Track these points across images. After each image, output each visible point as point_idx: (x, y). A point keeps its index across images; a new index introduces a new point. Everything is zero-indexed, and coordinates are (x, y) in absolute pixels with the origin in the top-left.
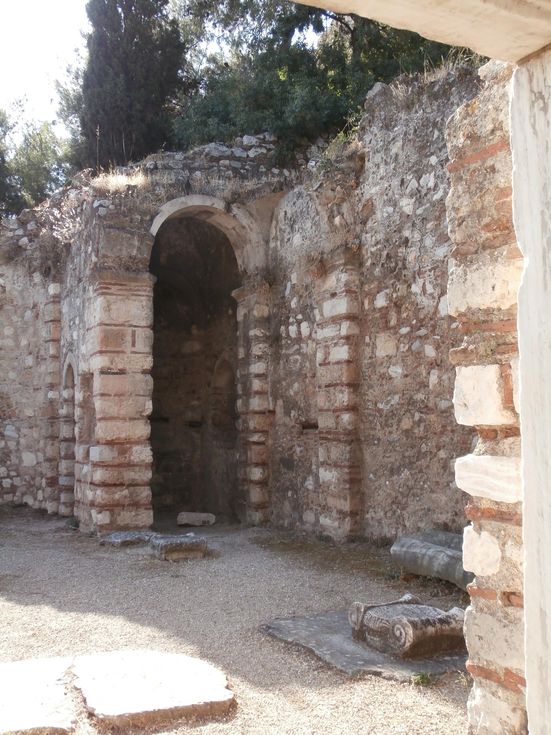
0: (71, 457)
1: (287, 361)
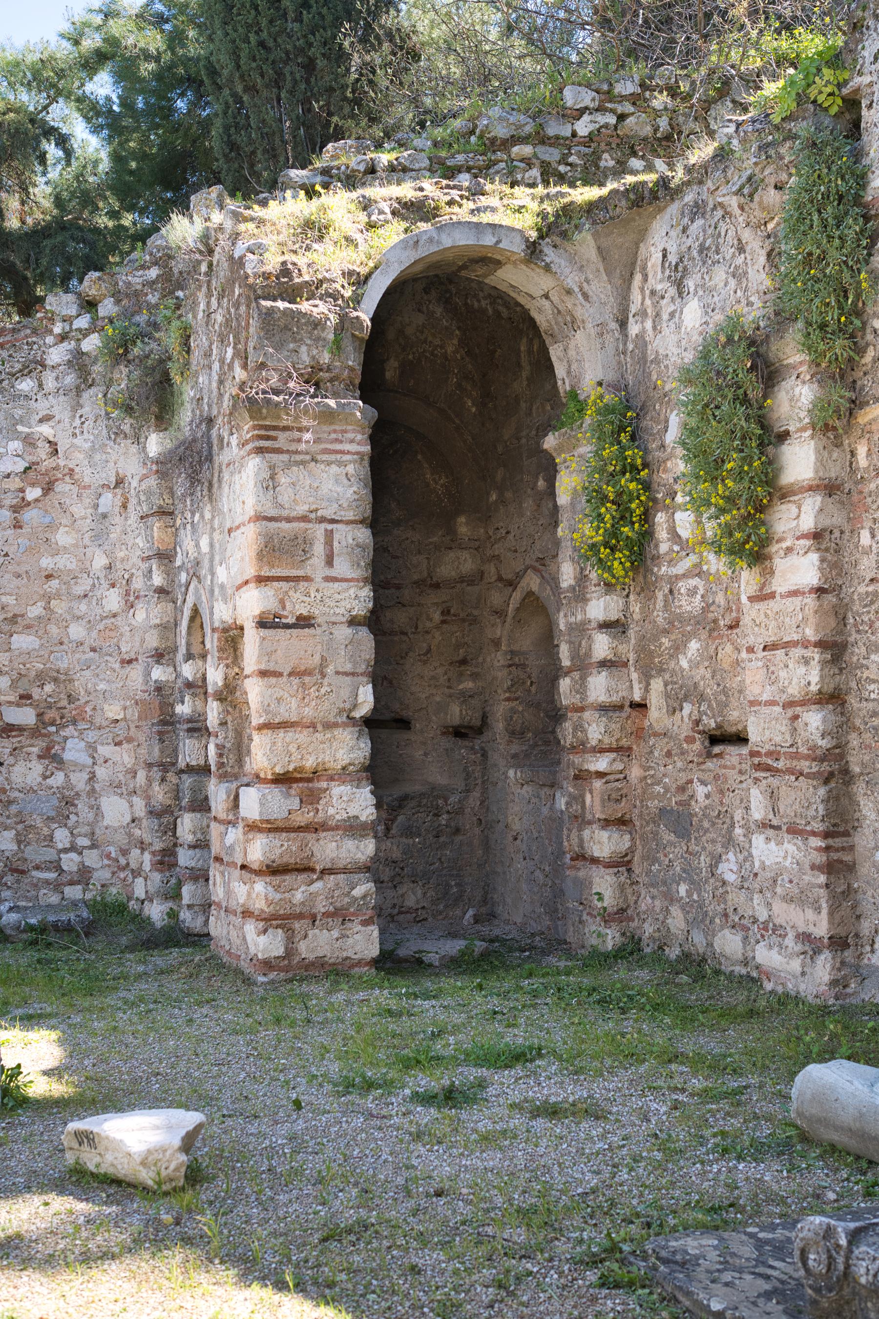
0: (201, 805)
1: (671, 591)
